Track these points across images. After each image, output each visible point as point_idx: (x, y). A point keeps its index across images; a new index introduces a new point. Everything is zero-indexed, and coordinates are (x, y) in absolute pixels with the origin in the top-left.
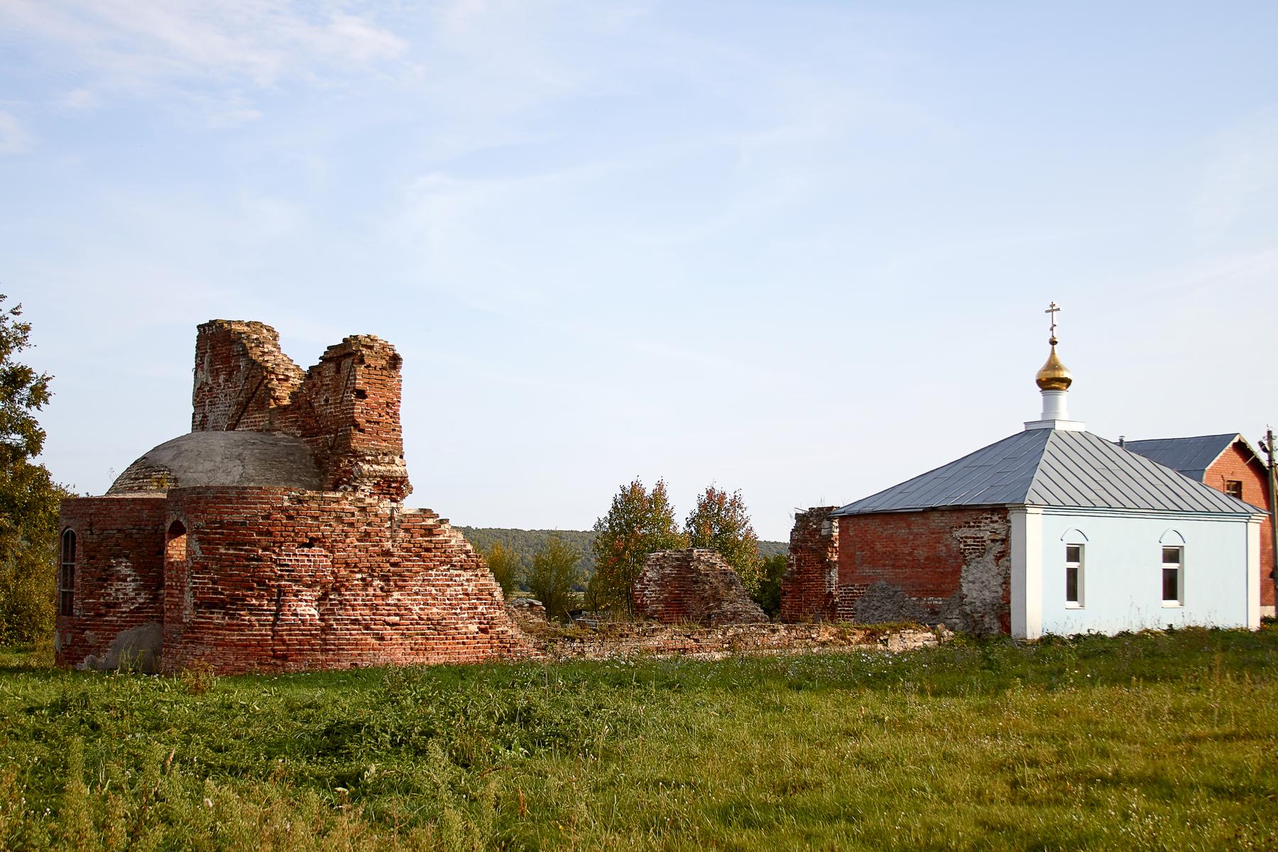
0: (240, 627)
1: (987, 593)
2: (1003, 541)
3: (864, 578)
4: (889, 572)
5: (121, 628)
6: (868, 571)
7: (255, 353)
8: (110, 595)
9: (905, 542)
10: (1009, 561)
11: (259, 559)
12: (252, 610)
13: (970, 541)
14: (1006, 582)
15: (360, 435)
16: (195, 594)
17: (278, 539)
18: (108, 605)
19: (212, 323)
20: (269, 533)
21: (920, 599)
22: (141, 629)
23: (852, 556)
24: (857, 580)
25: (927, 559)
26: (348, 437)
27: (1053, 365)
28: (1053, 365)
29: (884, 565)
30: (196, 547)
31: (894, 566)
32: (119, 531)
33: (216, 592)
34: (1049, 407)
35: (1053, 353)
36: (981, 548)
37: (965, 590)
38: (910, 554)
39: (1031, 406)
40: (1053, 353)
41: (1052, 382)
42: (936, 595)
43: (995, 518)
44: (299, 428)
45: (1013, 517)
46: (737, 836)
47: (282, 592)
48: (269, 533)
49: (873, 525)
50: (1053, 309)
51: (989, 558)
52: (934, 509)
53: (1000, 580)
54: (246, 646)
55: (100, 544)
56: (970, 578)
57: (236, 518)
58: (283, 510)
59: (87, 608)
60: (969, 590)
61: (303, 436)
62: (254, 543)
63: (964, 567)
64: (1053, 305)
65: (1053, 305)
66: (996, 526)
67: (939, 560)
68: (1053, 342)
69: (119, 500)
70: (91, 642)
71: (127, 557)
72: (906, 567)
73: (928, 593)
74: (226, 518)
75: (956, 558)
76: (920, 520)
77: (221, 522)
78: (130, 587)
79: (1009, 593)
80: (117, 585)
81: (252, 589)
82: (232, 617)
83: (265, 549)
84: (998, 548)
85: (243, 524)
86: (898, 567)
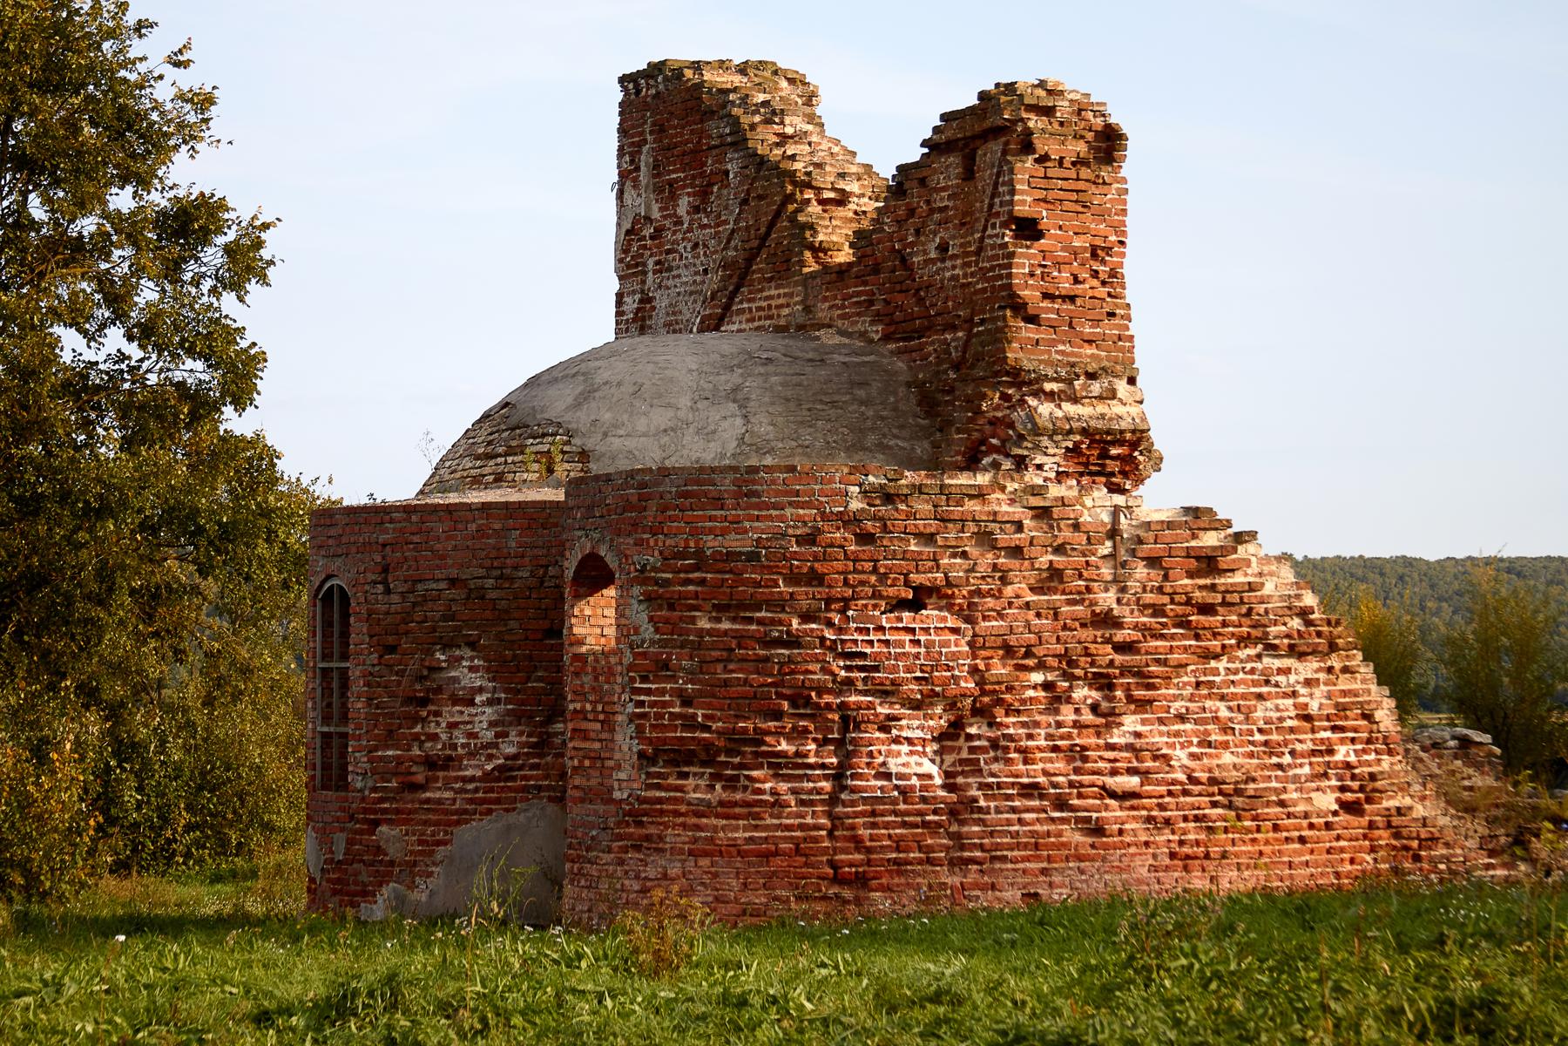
0: (752, 810)
5: (463, 817)
7: (763, 140)
8: (434, 737)
11: (793, 641)
12: (779, 765)
15: (1027, 332)
18: (431, 763)
20: (816, 578)
22: (512, 818)
32: (453, 582)
33: (690, 723)
48: (816, 578)
54: (767, 855)
55: (406, 617)
57: (734, 542)
58: (849, 520)
59: (380, 770)
61: (887, 338)
62: (779, 604)
69: (450, 509)
71: (472, 645)
74: (711, 543)
78: (483, 717)
80: (451, 713)
81: (778, 715)
85: (753, 557)
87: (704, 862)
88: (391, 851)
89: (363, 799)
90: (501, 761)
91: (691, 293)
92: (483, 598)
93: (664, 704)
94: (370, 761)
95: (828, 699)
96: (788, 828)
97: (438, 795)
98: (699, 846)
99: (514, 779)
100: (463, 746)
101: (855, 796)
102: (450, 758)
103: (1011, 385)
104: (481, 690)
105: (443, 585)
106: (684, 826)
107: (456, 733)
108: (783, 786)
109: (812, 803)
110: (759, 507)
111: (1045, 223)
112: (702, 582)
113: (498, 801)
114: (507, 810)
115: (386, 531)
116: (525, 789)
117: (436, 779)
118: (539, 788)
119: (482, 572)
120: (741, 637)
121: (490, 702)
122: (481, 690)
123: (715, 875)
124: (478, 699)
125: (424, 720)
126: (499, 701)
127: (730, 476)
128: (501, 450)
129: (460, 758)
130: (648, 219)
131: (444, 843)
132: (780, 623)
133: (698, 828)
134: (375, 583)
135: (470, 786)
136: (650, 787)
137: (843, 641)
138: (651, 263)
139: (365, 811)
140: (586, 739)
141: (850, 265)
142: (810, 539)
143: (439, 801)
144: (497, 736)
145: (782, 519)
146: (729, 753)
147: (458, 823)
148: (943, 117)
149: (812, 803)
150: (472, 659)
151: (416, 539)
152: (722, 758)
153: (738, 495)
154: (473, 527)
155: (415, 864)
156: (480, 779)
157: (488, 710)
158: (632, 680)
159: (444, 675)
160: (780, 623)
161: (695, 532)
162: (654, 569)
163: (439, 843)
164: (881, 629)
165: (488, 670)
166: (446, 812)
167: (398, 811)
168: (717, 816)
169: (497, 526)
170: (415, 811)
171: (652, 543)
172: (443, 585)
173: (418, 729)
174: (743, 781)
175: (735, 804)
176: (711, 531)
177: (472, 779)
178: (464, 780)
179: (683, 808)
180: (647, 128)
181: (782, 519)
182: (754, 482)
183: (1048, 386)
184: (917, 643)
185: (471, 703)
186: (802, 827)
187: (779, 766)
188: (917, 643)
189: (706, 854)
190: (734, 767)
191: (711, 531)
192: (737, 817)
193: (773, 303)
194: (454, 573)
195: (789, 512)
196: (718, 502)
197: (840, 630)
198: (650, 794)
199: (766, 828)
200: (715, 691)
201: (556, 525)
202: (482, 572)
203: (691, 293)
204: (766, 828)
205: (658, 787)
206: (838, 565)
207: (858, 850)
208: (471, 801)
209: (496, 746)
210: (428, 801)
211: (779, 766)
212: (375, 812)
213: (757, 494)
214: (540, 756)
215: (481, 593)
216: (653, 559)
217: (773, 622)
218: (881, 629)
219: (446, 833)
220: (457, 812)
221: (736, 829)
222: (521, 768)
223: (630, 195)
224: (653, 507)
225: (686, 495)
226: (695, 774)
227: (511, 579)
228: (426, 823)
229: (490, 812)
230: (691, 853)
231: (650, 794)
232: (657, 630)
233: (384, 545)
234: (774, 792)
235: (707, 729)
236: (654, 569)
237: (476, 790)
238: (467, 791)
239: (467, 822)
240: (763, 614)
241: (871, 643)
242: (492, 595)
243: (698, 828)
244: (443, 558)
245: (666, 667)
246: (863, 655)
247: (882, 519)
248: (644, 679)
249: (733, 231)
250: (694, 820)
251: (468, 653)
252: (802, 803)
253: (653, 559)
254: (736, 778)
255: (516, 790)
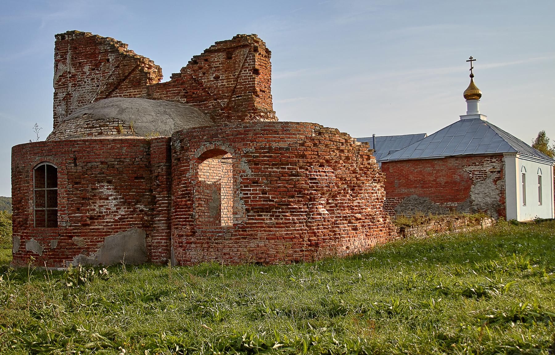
0: (287, 225)
1: (488, 199)
2: (499, 172)
3: (401, 194)
4: (419, 191)
5: (107, 233)
6: (404, 190)
7: (121, 50)
8: (94, 210)
9: (430, 174)
10: (505, 182)
11: (297, 175)
12: (293, 211)
13: (476, 173)
14: (502, 192)
15: (258, 99)
16: (246, 202)
17: (309, 160)
18: (92, 218)
19: (69, 33)
20: (303, 156)
21: (442, 204)
22: (126, 233)
23: (392, 183)
24: (396, 196)
25: (446, 183)
26: (252, 101)
27: (472, 86)
28: (472, 86)
29: (416, 187)
30: (244, 166)
31: (422, 187)
32: (102, 163)
33: (268, 199)
34: (472, 108)
35: (472, 81)
36: (484, 176)
37: (473, 198)
38: (435, 180)
39: (461, 108)
40: (472, 81)
41: (472, 95)
42: (453, 201)
43: (494, 160)
44: (184, 96)
45: (506, 160)
46: (323, 334)
47: (312, 199)
48: (303, 156)
49: (407, 166)
50: (471, 60)
51: (489, 181)
52: (452, 157)
53: (498, 192)
54: (292, 239)
55: (85, 173)
56: (476, 192)
57: (282, 145)
58: (312, 139)
59: (73, 220)
60: (475, 198)
61: (187, 102)
62: (295, 164)
63: (473, 186)
64: (471, 58)
65: (471, 58)
66: (494, 164)
67: (455, 183)
68: (472, 76)
69: (101, 141)
70: (80, 245)
71: (109, 182)
72: (431, 187)
73: (447, 200)
74: (274, 145)
75: (467, 181)
76: (441, 163)
77: (270, 148)
78: (112, 204)
79: (504, 198)
80: (99, 203)
81: (293, 197)
82: (277, 217)
83: (301, 168)
84: (496, 175)
85: (287, 149)
86: (426, 188)
87: (273, 241)
88: (79, 245)
89: (66, 229)
90: (120, 216)
91: (90, 92)
92: (113, 167)
93: (257, 194)
94: (69, 217)
95: (306, 192)
96: (298, 230)
97: (96, 227)
98: (271, 236)
99: (125, 222)
100: (105, 212)
101: (314, 220)
102: (100, 216)
103: (253, 113)
104: (111, 195)
105: (98, 164)
106: (265, 231)
107: (102, 208)
108: (295, 218)
109: (302, 223)
110: (289, 134)
111: (260, 71)
112: (271, 156)
113: (120, 228)
114: (124, 231)
115: (76, 147)
116: (129, 224)
117: (95, 223)
118: (135, 224)
119: (113, 160)
120: (283, 174)
121: (115, 199)
122: (111, 195)
123: (276, 245)
124: (110, 198)
125: (90, 205)
126: (117, 199)
127: (280, 125)
128: (98, 126)
129: (104, 216)
130: (70, 73)
131: (101, 242)
132: (295, 169)
133: (270, 231)
134: (70, 163)
135: (110, 224)
136: (249, 219)
137: (310, 175)
138: (70, 84)
139: (66, 233)
140: (201, 206)
141: (169, 82)
142: (302, 145)
143: (98, 229)
144: (117, 209)
145: (296, 138)
146: (277, 208)
147: (106, 235)
148: (216, 43)
149: (302, 223)
150: (108, 186)
151: (88, 150)
152: (274, 210)
153: (283, 130)
154: (109, 146)
155: (89, 248)
156: (113, 222)
157: (114, 201)
158: (241, 187)
159: (97, 191)
160: (295, 169)
161: (268, 141)
162: (252, 153)
163: (98, 242)
164: (319, 171)
165: (115, 189)
166: (101, 232)
167: (80, 233)
168: (275, 227)
169: (118, 146)
170: (89, 232)
171: (251, 144)
172: (98, 164)
173: (88, 207)
174: (281, 217)
175: (280, 224)
176: (274, 141)
177: (110, 222)
178: (107, 222)
179: (264, 225)
180: (69, 48)
181: (296, 138)
182: (288, 127)
183: (262, 114)
184: (326, 175)
185: (107, 199)
186: (301, 230)
187: (294, 212)
188: (326, 175)
189: (273, 239)
190: (279, 212)
191: (274, 141)
192: (282, 227)
193: (132, 94)
194: (103, 160)
195: (298, 136)
196: (276, 132)
197: (310, 172)
198: (250, 221)
199: (291, 230)
200: (275, 190)
201: (138, 146)
202: (113, 160)
203: (90, 92)
204: (291, 230)
205: (253, 219)
206: (310, 153)
207: (315, 236)
208: (109, 229)
209: (117, 212)
210: (93, 229)
211: (294, 212)
212: (71, 233)
213: (287, 130)
214: (132, 215)
215: (113, 166)
216: (252, 149)
217: (293, 169)
218: (319, 171)
219: (101, 238)
220: (105, 232)
221: (282, 231)
222: (127, 218)
223: (61, 66)
224: (251, 135)
225: (265, 130)
226: (265, 215)
227: (123, 162)
228: (93, 236)
229: (117, 232)
230: (267, 239)
231: (250, 221)
232: (252, 172)
233: (74, 152)
234: (293, 220)
235: (273, 201)
236: (252, 153)
237: (112, 225)
238: (108, 226)
239: (109, 235)
240: (289, 166)
241: (317, 175)
242: (118, 166)
243: (270, 231)
244: (99, 155)
245: (257, 182)
246: (316, 179)
247: (319, 139)
248: (245, 187)
249: (111, 75)
250: (268, 229)
251: (106, 184)
252: (300, 223)
253: (252, 149)
254: (279, 216)
255: (126, 225)
